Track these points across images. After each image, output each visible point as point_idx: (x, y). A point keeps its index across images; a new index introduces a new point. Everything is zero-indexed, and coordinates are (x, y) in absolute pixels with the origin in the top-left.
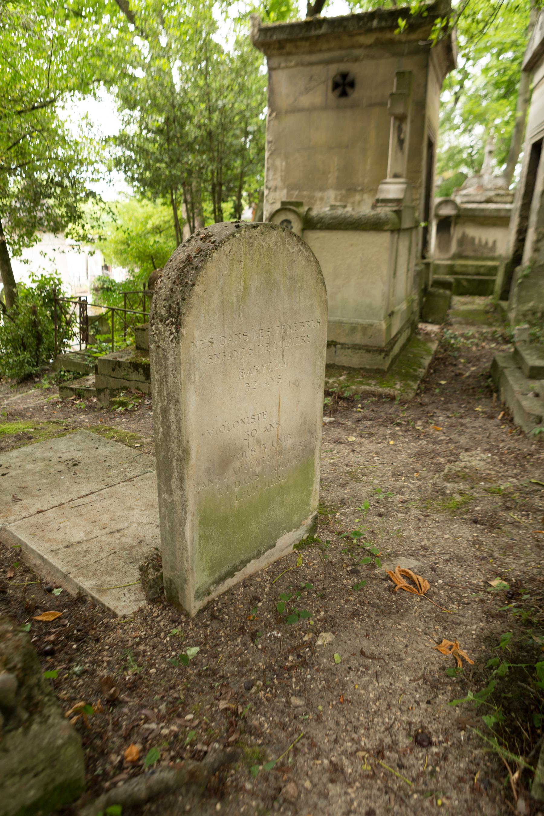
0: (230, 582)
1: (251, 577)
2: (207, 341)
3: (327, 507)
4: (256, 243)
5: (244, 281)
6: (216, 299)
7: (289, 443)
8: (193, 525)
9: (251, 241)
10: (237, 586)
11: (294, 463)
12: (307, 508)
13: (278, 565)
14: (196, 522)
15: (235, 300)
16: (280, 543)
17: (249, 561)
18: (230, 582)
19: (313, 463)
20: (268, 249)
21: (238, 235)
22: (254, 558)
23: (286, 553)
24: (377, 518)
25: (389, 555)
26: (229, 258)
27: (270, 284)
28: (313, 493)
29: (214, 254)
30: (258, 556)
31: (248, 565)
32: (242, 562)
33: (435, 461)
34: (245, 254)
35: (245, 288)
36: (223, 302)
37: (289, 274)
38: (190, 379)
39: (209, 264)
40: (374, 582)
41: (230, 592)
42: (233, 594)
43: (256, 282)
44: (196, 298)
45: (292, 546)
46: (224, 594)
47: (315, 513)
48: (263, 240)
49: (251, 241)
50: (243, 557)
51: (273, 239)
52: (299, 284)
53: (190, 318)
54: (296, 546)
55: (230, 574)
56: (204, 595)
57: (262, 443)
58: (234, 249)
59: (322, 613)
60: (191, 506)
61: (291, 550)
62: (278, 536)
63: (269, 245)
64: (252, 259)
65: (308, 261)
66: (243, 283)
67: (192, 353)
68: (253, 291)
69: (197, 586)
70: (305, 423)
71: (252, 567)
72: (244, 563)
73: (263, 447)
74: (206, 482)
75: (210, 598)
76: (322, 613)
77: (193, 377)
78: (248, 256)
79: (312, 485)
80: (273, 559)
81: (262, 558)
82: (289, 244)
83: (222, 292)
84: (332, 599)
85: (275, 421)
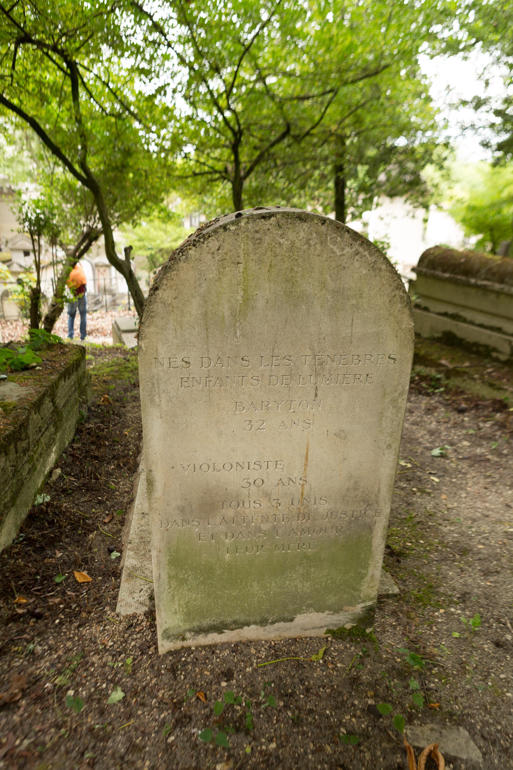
0: (213, 638)
1: (248, 644)
2: (179, 360)
3: (437, 593)
4: (267, 239)
5: (245, 290)
6: (194, 308)
7: (323, 507)
8: (159, 563)
9: (258, 236)
10: (224, 646)
11: (333, 534)
12: (356, 593)
13: (291, 645)
14: (165, 560)
15: (227, 313)
16: (300, 619)
17: (248, 624)
18: (213, 638)
19: (369, 544)
20: (292, 247)
21: (233, 228)
22: (255, 623)
23: (313, 633)
24: (488, 647)
25: (451, 714)
26: (217, 258)
27: (292, 296)
28: (368, 579)
29: (191, 252)
30: (263, 622)
31: (246, 628)
32: (235, 622)
33: (32, 734)
34: (247, 254)
35: (246, 300)
36: (206, 314)
37: (331, 284)
38: (152, 401)
39: (181, 264)
40: (384, 744)
41: (212, 648)
42: (213, 653)
43: (265, 292)
44: (160, 305)
45: (325, 629)
46: (204, 647)
47: (370, 603)
48: (282, 236)
49: (258, 236)
50: (242, 618)
51: (302, 234)
52: (354, 302)
53: (152, 329)
54: (329, 631)
55: (219, 629)
56: (177, 638)
57: (274, 497)
58: (226, 246)
59: (273, 745)
60: (157, 540)
61: (321, 633)
62: (298, 611)
63: (293, 243)
64: (260, 261)
65: (373, 268)
66: (242, 293)
67: (154, 371)
68: (261, 304)
69: (167, 626)
70: (356, 489)
71: (251, 632)
72: (240, 625)
73: (274, 503)
74: (179, 522)
75: (186, 644)
76: (273, 745)
77: (157, 399)
78: (252, 256)
79: (366, 567)
80: (288, 634)
81: (269, 627)
82: (335, 243)
83: (205, 302)
84: (304, 733)
85: (296, 474)
